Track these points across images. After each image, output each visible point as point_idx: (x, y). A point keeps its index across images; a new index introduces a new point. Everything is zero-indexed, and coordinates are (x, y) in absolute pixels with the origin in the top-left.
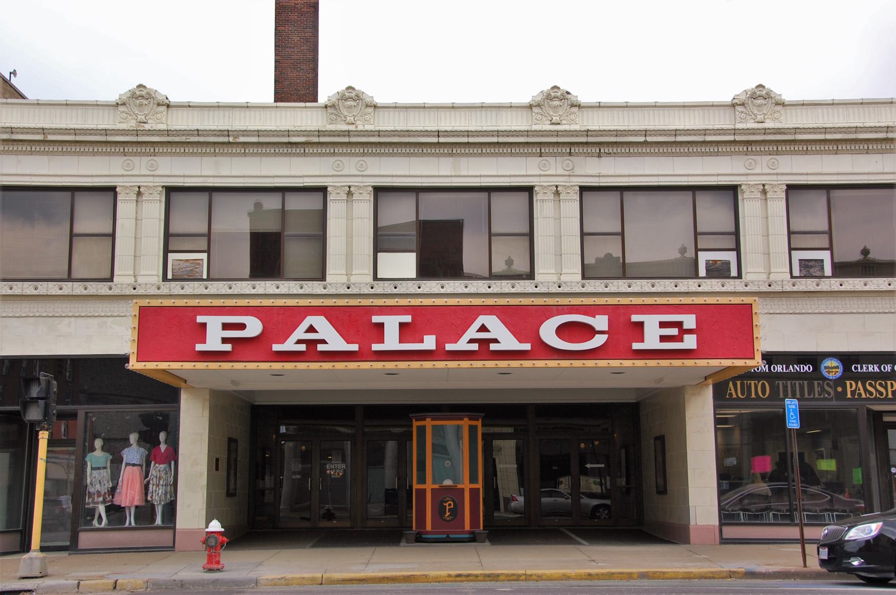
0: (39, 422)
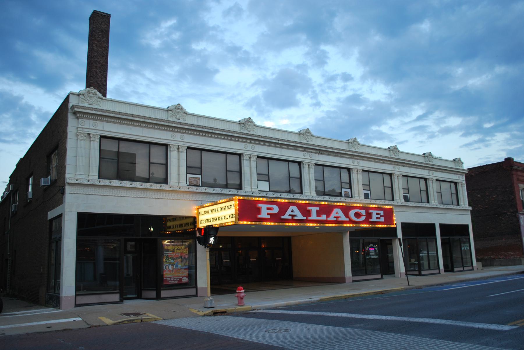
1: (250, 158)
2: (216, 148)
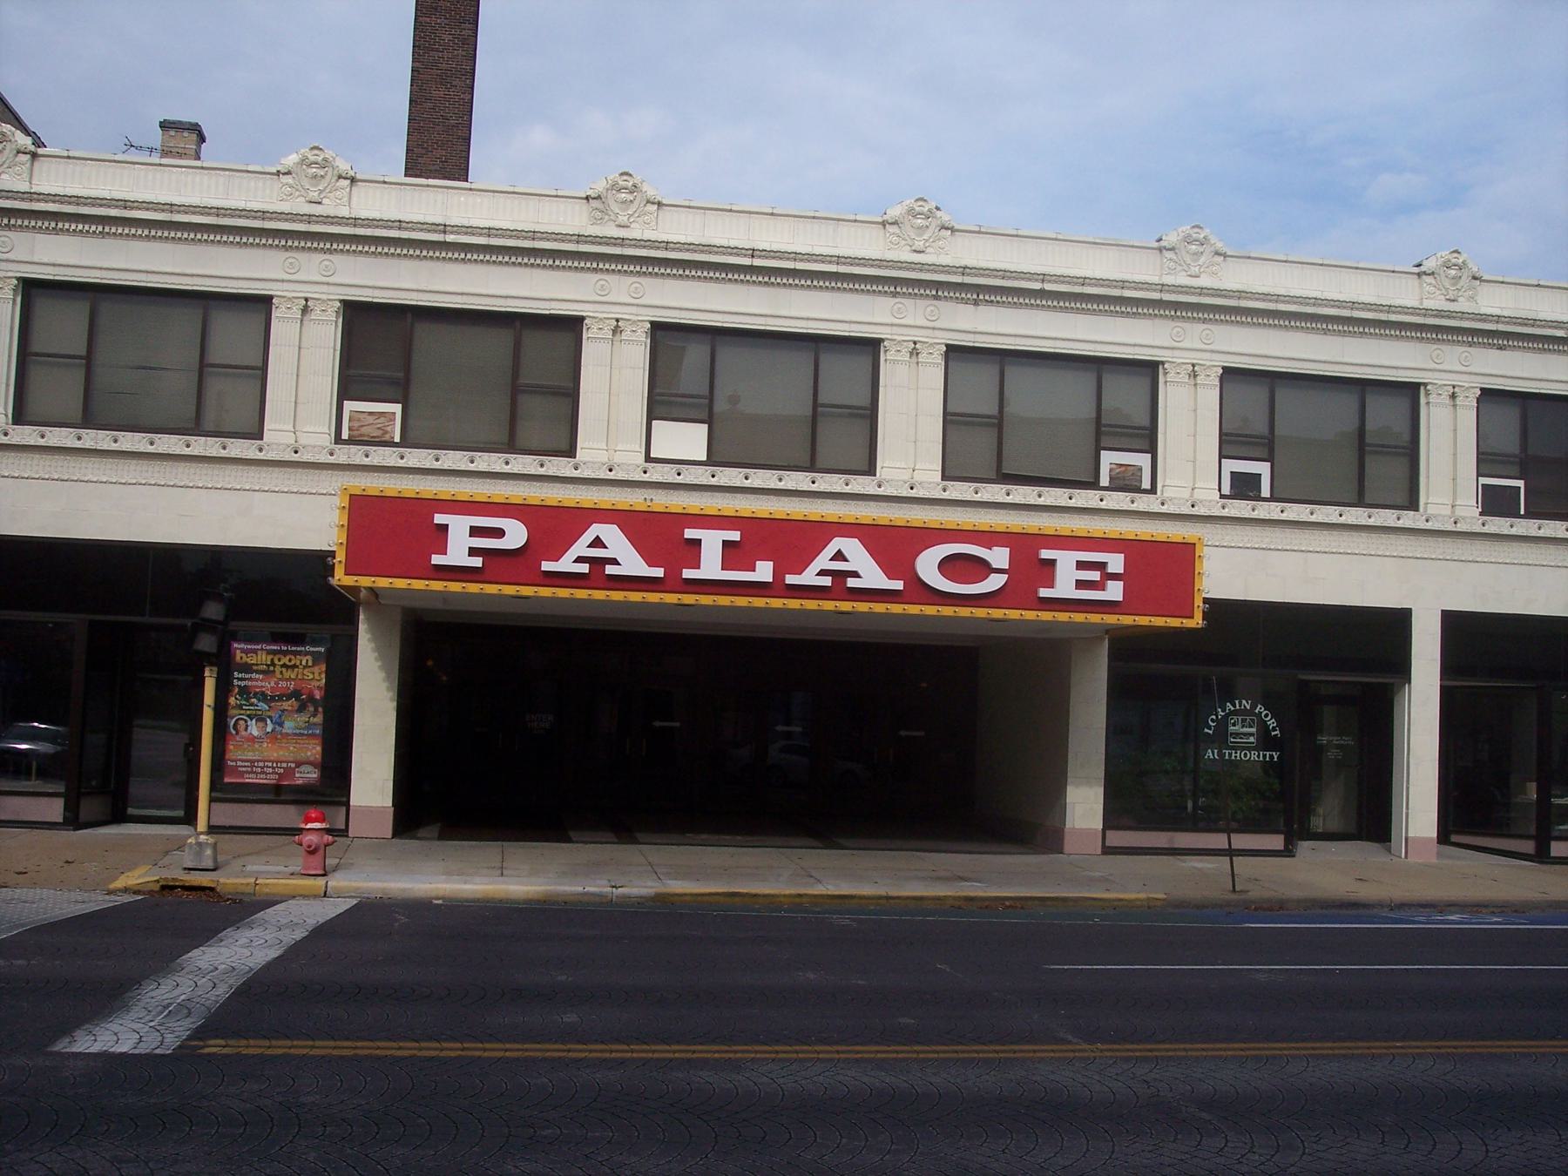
0: (208, 655)
1: (1453, 396)
2: (1543, 385)
